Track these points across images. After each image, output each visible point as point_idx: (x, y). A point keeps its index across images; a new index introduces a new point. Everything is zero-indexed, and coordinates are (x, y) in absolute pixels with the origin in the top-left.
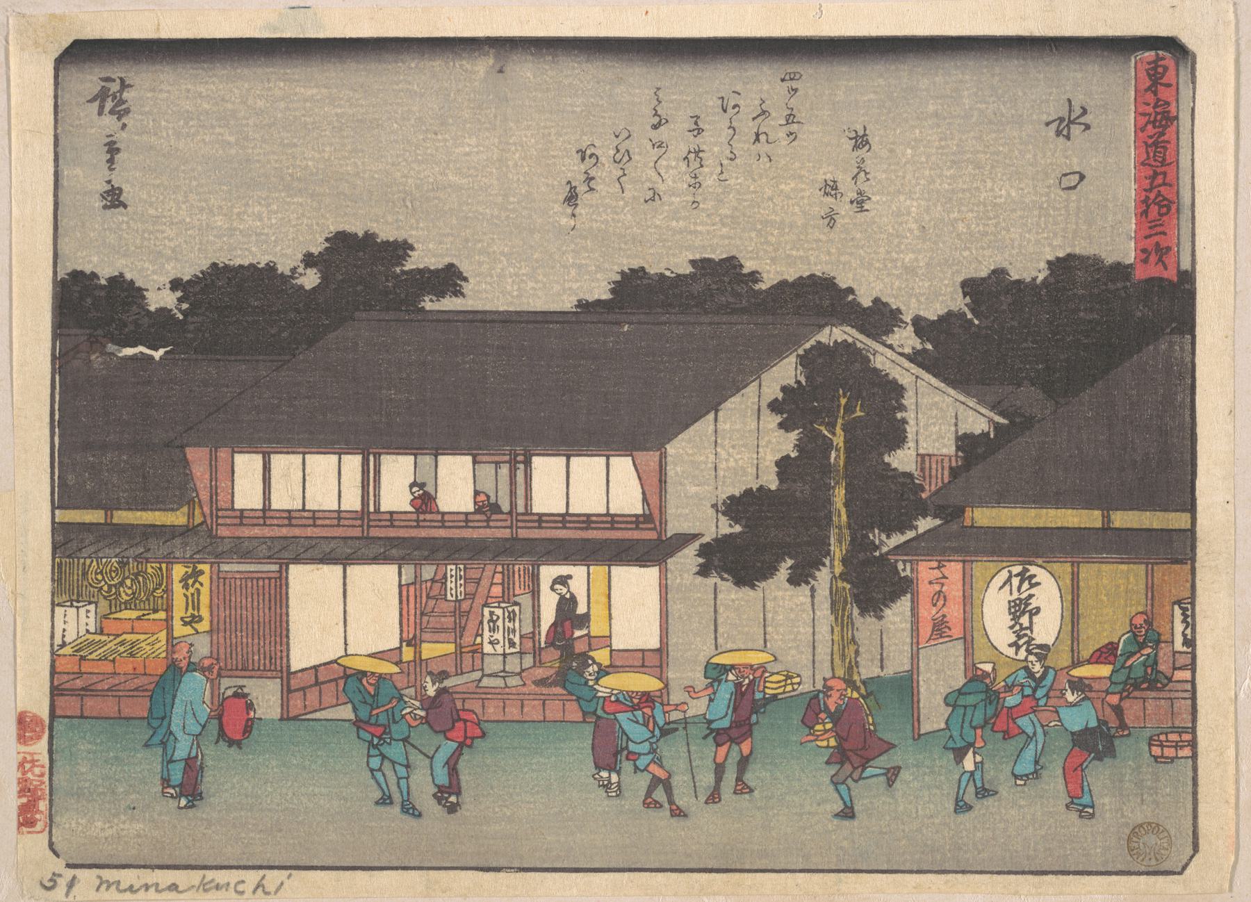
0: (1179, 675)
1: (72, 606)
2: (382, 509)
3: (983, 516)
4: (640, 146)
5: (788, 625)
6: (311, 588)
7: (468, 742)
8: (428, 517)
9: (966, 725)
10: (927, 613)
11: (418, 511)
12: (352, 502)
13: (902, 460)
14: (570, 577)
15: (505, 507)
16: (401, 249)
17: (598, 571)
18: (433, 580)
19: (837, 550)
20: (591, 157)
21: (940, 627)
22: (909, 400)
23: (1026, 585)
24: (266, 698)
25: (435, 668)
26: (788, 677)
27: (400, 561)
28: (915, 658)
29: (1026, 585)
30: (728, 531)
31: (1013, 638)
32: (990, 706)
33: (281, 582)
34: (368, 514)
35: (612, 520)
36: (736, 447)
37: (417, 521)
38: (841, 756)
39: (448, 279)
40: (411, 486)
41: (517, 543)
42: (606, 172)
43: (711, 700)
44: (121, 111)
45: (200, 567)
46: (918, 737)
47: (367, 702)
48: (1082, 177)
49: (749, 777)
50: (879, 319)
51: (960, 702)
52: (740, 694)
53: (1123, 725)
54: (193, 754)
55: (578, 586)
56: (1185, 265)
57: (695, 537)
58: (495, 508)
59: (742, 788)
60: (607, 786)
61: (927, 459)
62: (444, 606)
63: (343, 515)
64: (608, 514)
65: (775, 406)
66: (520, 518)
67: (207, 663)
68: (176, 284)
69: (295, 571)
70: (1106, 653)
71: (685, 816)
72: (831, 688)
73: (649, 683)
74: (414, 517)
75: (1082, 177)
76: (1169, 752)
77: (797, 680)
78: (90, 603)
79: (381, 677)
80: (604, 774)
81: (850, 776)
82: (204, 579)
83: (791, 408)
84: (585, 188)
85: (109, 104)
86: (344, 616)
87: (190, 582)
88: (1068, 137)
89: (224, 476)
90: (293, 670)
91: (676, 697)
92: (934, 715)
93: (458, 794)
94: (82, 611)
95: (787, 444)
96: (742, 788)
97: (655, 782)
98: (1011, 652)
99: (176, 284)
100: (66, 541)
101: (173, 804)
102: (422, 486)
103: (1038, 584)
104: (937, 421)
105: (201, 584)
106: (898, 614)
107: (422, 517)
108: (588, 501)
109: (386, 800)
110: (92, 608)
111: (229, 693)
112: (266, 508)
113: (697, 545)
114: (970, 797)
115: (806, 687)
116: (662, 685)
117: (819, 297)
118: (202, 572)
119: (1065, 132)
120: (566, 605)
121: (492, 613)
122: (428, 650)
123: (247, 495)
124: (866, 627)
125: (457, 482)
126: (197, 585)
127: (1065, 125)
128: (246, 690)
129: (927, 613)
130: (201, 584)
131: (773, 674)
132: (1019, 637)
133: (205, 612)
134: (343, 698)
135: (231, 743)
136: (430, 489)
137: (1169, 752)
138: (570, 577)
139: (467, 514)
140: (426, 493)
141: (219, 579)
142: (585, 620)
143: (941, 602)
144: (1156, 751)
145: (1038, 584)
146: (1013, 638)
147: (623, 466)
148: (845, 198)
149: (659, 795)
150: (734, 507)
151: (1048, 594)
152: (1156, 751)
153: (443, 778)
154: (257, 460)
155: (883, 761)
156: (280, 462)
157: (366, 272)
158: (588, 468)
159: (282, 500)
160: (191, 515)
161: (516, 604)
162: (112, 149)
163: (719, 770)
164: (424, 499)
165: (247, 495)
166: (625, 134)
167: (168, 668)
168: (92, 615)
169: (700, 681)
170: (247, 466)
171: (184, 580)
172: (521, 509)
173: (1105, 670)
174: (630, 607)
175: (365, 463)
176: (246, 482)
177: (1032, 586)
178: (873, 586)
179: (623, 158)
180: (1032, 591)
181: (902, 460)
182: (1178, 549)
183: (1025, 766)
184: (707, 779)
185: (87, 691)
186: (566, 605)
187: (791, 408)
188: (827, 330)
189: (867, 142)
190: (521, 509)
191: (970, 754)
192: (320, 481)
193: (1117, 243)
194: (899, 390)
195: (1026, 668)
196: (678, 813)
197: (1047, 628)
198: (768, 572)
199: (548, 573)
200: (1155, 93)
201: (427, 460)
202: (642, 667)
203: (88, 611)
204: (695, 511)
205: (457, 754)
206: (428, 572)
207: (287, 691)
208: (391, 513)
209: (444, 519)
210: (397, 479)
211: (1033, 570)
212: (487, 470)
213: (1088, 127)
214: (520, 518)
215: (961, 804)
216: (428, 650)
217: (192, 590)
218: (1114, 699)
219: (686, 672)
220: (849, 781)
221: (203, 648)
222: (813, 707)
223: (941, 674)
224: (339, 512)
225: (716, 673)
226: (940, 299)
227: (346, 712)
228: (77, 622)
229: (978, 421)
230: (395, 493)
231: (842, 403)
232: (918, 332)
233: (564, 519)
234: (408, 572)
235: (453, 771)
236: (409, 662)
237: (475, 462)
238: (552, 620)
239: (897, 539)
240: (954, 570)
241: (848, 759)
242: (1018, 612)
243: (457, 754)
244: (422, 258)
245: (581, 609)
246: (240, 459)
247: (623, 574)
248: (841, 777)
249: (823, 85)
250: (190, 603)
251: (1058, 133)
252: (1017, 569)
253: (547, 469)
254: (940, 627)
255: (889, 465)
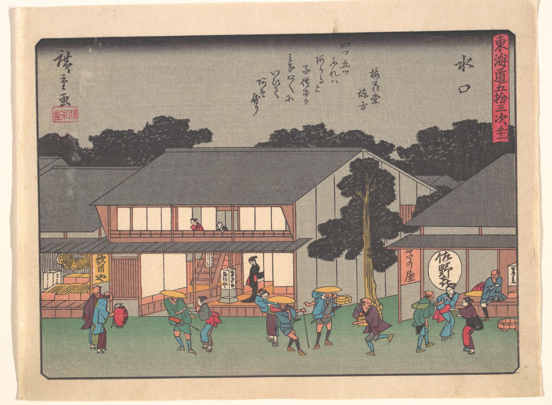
0: (511, 295)
1: (50, 273)
2: (179, 229)
3: (429, 231)
4: (283, 78)
5: (347, 276)
6: (150, 263)
7: (216, 325)
8: (199, 232)
9: (421, 317)
10: (405, 269)
11: (194, 230)
12: (167, 227)
13: (394, 207)
14: (256, 257)
15: (230, 228)
16: (185, 123)
17: (268, 256)
18: (201, 259)
19: (367, 244)
20: (263, 83)
21: (410, 276)
22: (396, 182)
23: (446, 259)
24: (132, 307)
25: (201, 295)
26: (347, 298)
27: (186, 252)
28: (400, 291)
29: (446, 259)
30: (321, 237)
31: (441, 281)
32: (433, 309)
33: (138, 259)
34: (174, 231)
35: (273, 233)
36: (325, 203)
37: (194, 234)
38: (369, 329)
39: (205, 135)
40: (191, 220)
41: (232, 243)
42: (269, 90)
43: (315, 307)
44: (68, 65)
45: (104, 255)
46: (400, 321)
47: (174, 311)
48: (469, 87)
49: (330, 339)
50: (384, 149)
51: (419, 307)
52: (326, 303)
53: (487, 316)
54: (102, 332)
55: (259, 261)
56: (512, 123)
57: (310, 239)
58: (225, 228)
59: (328, 343)
60: (272, 341)
61: (410, 207)
62: (203, 269)
63: (163, 232)
64: (272, 230)
65: (340, 186)
66: (235, 232)
67: (108, 294)
68: (91, 138)
69: (143, 256)
70: (481, 287)
71: (305, 354)
72: (364, 302)
73: (290, 301)
74: (192, 232)
75: (469, 87)
76: (507, 327)
77: (350, 299)
78: (59, 271)
79: (178, 299)
80: (272, 337)
81: (373, 339)
82: (106, 260)
83: (345, 186)
84: (261, 95)
85: (62, 63)
86: (163, 275)
87: (100, 261)
88: (463, 70)
89: (112, 218)
90: (143, 297)
91: (301, 305)
92: (408, 313)
93: (212, 345)
94: (55, 274)
95: (345, 201)
96: (328, 343)
97: (292, 341)
98: (440, 286)
99: (91, 138)
100: (44, 247)
101: (95, 351)
102: (195, 220)
103: (451, 258)
104: (408, 190)
105: (105, 262)
106: (393, 270)
107: (195, 232)
108: (263, 225)
109: (182, 347)
110: (59, 273)
111: (117, 306)
112: (131, 230)
113: (307, 244)
114: (423, 346)
115: (354, 301)
116: (294, 301)
117: (356, 139)
118: (105, 257)
119: (462, 68)
120: (255, 269)
121: (224, 273)
122: (199, 288)
123: (123, 224)
124: (378, 276)
125: (209, 218)
126: (103, 263)
127: (461, 66)
128: (123, 305)
129: (405, 269)
130: (105, 262)
131: (340, 296)
132: (444, 280)
133: (106, 273)
134: (164, 308)
135: (118, 327)
136: (199, 221)
137: (507, 327)
138: (256, 257)
139: (214, 231)
140: (197, 223)
141: (112, 259)
142: (262, 275)
143: (410, 265)
144: (501, 326)
145: (451, 258)
146: (441, 281)
147: (277, 211)
148: (370, 97)
149: (294, 346)
150: (322, 228)
151: (455, 261)
152: (501, 326)
153: (205, 339)
154: (128, 210)
155: (386, 332)
156: (137, 211)
157: (171, 134)
158: (263, 212)
159: (139, 226)
160: (100, 234)
161: (235, 269)
162: (64, 80)
163: (319, 334)
164: (197, 227)
165: (123, 224)
166: (277, 72)
167: (91, 298)
168: (59, 276)
169: (311, 299)
170: (123, 213)
171: (98, 259)
172: (236, 229)
173: (479, 293)
174: (279, 269)
175: (172, 211)
176: (123, 219)
177: (449, 259)
178: (382, 260)
179: (276, 84)
180: (448, 261)
181: (394, 207)
182: (512, 243)
183: (447, 333)
184: (313, 339)
185: (56, 308)
186: (255, 269)
187: (345, 186)
188: (361, 154)
189: (378, 74)
190: (236, 229)
191: (423, 329)
192: (153, 219)
193: (483, 114)
194: (393, 178)
195: (447, 293)
196: (302, 353)
197: (454, 277)
198: (338, 255)
199: (247, 256)
200: (500, 51)
201: (197, 210)
202: (286, 294)
203: (58, 274)
204: (308, 231)
205: (211, 330)
206: (198, 256)
207: (140, 306)
208: (182, 231)
209: (205, 233)
210: (185, 218)
211: (450, 252)
212: (221, 213)
213: (472, 66)
214: (235, 232)
215: (419, 349)
216: (199, 288)
217: (101, 264)
218: (484, 305)
219: (305, 295)
220: (373, 341)
221: (105, 289)
222: (358, 310)
223: (411, 295)
224: (161, 231)
225: (317, 296)
226: (408, 140)
227: (165, 313)
228: (51, 279)
229: (425, 191)
230: (185, 222)
231: (368, 184)
232: (400, 155)
233: (253, 233)
234: (190, 256)
235: (209, 335)
236: (190, 293)
237: (217, 211)
238: (249, 275)
239: (391, 242)
240: (416, 253)
241: (372, 330)
242: (445, 271)
243: (211, 330)
244: (193, 126)
245: (261, 271)
246: (120, 210)
247: (278, 256)
248: (369, 339)
249: (353, 56)
250: (99, 273)
251: (460, 68)
252: (443, 252)
253: (246, 213)
254: (410, 276)
255: (389, 210)
